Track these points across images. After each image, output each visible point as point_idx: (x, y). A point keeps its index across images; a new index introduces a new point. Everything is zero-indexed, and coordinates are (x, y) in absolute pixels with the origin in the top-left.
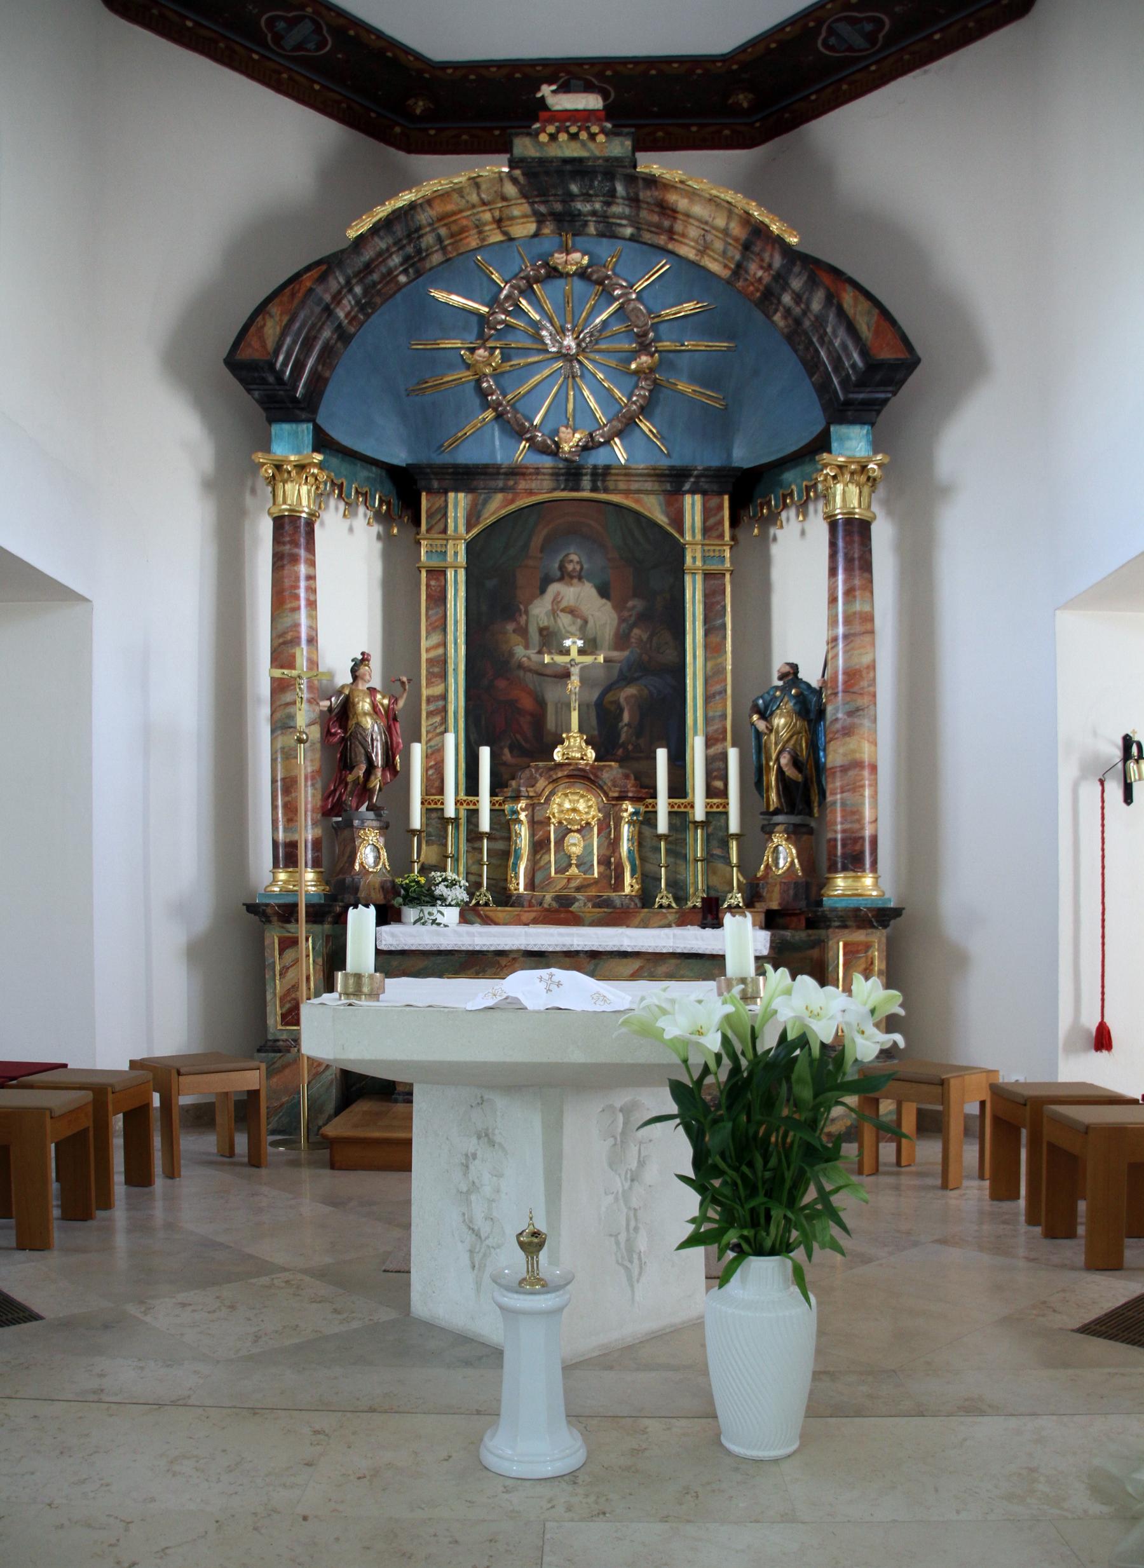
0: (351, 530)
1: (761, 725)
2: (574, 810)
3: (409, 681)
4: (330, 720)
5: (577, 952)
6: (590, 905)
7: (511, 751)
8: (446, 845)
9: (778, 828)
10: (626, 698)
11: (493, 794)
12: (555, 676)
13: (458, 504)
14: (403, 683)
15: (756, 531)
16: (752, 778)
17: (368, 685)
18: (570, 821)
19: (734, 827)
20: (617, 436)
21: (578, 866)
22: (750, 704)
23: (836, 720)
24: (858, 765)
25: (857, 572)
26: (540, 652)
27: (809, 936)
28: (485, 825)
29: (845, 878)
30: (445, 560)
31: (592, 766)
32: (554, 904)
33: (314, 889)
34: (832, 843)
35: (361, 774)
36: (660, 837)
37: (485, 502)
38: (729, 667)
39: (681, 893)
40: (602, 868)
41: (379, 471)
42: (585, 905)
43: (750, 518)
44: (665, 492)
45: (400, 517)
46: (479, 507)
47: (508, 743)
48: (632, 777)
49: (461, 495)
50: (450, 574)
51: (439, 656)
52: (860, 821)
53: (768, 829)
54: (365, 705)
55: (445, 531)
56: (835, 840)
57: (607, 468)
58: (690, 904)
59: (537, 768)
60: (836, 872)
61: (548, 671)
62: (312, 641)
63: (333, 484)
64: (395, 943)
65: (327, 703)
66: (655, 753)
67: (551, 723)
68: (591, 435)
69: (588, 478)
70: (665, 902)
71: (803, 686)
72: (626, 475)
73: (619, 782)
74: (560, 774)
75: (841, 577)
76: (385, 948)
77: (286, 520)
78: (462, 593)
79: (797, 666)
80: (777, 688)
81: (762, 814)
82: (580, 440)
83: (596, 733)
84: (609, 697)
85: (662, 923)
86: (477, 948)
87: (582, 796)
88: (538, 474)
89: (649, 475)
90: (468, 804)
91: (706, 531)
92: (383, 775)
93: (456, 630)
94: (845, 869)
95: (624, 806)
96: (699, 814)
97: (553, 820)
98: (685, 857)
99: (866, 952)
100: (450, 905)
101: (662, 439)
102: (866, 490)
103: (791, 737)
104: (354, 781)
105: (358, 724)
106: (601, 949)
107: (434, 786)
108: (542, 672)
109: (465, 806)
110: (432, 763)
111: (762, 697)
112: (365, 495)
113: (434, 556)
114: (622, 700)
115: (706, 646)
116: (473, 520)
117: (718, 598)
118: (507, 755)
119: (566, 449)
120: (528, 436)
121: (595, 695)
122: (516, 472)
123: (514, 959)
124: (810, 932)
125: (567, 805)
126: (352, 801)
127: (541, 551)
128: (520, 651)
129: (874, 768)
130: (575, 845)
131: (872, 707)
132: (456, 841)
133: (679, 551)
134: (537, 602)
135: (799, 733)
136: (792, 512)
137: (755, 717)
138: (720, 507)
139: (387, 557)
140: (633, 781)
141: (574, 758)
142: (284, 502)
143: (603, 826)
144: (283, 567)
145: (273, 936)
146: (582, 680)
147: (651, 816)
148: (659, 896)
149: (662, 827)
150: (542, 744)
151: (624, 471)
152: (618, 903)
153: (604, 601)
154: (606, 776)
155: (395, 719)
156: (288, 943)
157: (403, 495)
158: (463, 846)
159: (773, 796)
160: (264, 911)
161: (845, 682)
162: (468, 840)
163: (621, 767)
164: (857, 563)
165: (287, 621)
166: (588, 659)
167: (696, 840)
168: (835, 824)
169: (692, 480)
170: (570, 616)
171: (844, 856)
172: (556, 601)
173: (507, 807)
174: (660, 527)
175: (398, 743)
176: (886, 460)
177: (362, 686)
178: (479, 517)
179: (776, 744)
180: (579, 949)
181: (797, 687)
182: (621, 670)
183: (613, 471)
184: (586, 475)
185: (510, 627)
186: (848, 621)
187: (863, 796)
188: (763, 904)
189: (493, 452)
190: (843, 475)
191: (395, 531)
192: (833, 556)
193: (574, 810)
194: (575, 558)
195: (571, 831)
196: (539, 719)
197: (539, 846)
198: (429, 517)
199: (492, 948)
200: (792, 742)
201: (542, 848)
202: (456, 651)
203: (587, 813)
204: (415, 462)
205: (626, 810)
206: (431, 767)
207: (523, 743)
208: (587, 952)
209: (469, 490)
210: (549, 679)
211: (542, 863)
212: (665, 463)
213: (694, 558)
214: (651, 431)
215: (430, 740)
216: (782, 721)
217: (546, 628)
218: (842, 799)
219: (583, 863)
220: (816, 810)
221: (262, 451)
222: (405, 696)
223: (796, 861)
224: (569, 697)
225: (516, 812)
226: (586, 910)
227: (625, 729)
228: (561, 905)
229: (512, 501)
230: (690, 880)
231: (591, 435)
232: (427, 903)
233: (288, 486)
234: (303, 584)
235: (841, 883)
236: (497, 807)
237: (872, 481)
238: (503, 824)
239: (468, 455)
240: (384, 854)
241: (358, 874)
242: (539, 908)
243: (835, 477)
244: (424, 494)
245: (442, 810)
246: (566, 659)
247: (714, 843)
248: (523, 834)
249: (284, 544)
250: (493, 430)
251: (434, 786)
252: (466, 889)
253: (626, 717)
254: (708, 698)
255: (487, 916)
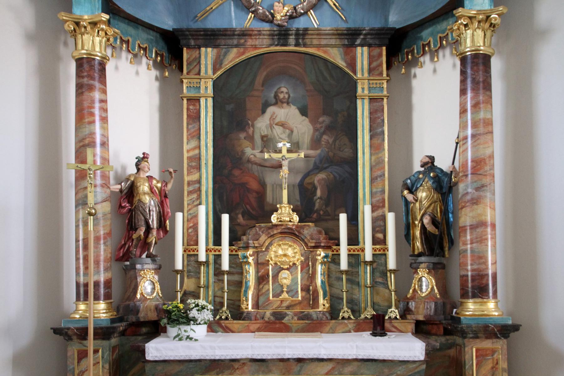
0: (137, 73)
1: (410, 197)
2: (285, 255)
3: (175, 171)
4: (122, 197)
5: (288, 359)
6: (296, 318)
7: (243, 217)
8: (199, 278)
9: (422, 265)
10: (318, 181)
11: (231, 244)
12: (272, 167)
13: (208, 55)
14: (170, 173)
15: (403, 71)
16: (403, 233)
17: (147, 174)
18: (283, 263)
19: (392, 264)
20: (311, 9)
21: (287, 292)
22: (402, 183)
23: (467, 193)
24: (483, 224)
25: (481, 91)
26: (262, 152)
27: (447, 340)
28: (225, 266)
29: (475, 302)
30: (199, 92)
31: (297, 226)
32: (272, 318)
33: (104, 315)
34: (464, 278)
35: (142, 233)
36: (342, 272)
37: (225, 54)
38: (386, 160)
39: (356, 308)
40: (304, 293)
41: (155, 34)
42: (293, 318)
43: (399, 62)
44: (344, 45)
45: (170, 65)
46: (222, 57)
47: (241, 211)
48: (323, 232)
49: (209, 50)
50: (203, 101)
51: (196, 155)
52: (486, 263)
53: (414, 265)
54: (144, 187)
55: (199, 73)
56: (467, 276)
57: (306, 30)
58: (363, 316)
59: (260, 228)
60: (468, 298)
61: (267, 164)
62: (104, 144)
63: (122, 41)
64: (158, 355)
65: (119, 187)
66: (339, 216)
67: (269, 198)
68: (295, 8)
69: (293, 37)
70: (346, 315)
71: (437, 170)
72: (318, 34)
73: (315, 236)
74: (275, 232)
75: (469, 95)
76: (151, 359)
77: (85, 61)
78: (210, 114)
79: (433, 157)
80: (419, 172)
81: (411, 256)
82: (288, 11)
83: (299, 203)
84: (307, 180)
85: (344, 330)
86: (217, 358)
87: (290, 246)
88: (260, 35)
89: (333, 34)
90: (215, 251)
91: (370, 71)
92: (158, 233)
93: (207, 138)
94: (474, 296)
95: (318, 252)
96: (368, 257)
97: (271, 262)
98: (358, 284)
99: (492, 356)
100: (200, 324)
101: (342, 10)
102: (489, 33)
103: (431, 204)
104: (137, 238)
105: (140, 201)
106: (305, 357)
107: (191, 240)
108: (262, 165)
109: (213, 253)
110: (191, 225)
111: (410, 179)
112: (145, 49)
113: (192, 90)
114: (316, 182)
115: (371, 146)
116: (218, 66)
117: (379, 115)
118: (240, 219)
119: (279, 18)
120: (253, 9)
121: (298, 179)
122: (245, 34)
123: (244, 363)
124: (448, 337)
125: (280, 252)
126: (136, 251)
127: (263, 86)
128: (249, 151)
129: (493, 226)
130: (285, 278)
131: (492, 184)
132: (206, 276)
133: (353, 84)
134: (260, 119)
135: (435, 202)
136: (427, 58)
137: (406, 192)
138: (380, 55)
139: (163, 92)
140: (324, 236)
141: (285, 221)
142: (83, 49)
143: (305, 265)
144: (82, 93)
145: (74, 348)
146: (290, 170)
147: (336, 257)
148: (342, 311)
149: (344, 265)
150: (262, 212)
151: (317, 32)
152: (315, 316)
153: (304, 117)
154: (306, 232)
155: (166, 196)
156: (83, 355)
157: (172, 49)
158: (212, 279)
159: (418, 244)
160: (66, 333)
161: (473, 168)
162: (215, 275)
163: (316, 226)
164: (481, 85)
165: (86, 130)
166: (293, 156)
167: (365, 273)
168: (466, 265)
169: (362, 37)
170: (281, 128)
171: (473, 287)
172: (272, 118)
173: (240, 253)
174: (341, 69)
175: (168, 213)
176: (505, 11)
177: (143, 175)
178: (221, 64)
179: (420, 210)
180: (290, 357)
181: (434, 172)
182: (315, 163)
183: (310, 32)
184: (292, 35)
185: (242, 135)
186: (475, 125)
187: (487, 245)
188: (412, 316)
189: (231, 21)
190: (472, 23)
191: (167, 74)
192: (463, 82)
193: (285, 255)
194: (284, 90)
195: (283, 269)
196: (261, 195)
197: (262, 279)
198: (188, 64)
199: (228, 358)
200: (431, 208)
201: (263, 280)
202: (207, 151)
203: (294, 257)
204: (179, 27)
205: (320, 255)
206: (190, 227)
207: (251, 211)
208: (294, 359)
209: (215, 46)
210: (267, 169)
211: (264, 291)
212: (343, 26)
213: (363, 89)
214: (334, 4)
215: (190, 210)
216: (424, 194)
217: (266, 136)
218: (471, 248)
219: (291, 291)
220: (446, 253)
221: (65, 11)
222: (172, 181)
223: (435, 287)
224: (281, 180)
225: (246, 257)
226: (293, 321)
227: (318, 201)
228: (277, 319)
229: (243, 53)
230: (362, 298)
231: (295, 8)
232: (184, 323)
233: (86, 37)
234: (97, 105)
235: (471, 307)
236: (234, 253)
237: (492, 25)
238: (237, 265)
239: (214, 22)
240: (158, 287)
241: (139, 301)
242: (261, 321)
243: (466, 26)
244: (185, 49)
245: (197, 255)
246: (279, 156)
247: (377, 274)
248: (251, 271)
249: (83, 77)
250: (230, 5)
251: (191, 240)
252: (211, 310)
253: (319, 193)
254: (373, 180)
255: (227, 327)
